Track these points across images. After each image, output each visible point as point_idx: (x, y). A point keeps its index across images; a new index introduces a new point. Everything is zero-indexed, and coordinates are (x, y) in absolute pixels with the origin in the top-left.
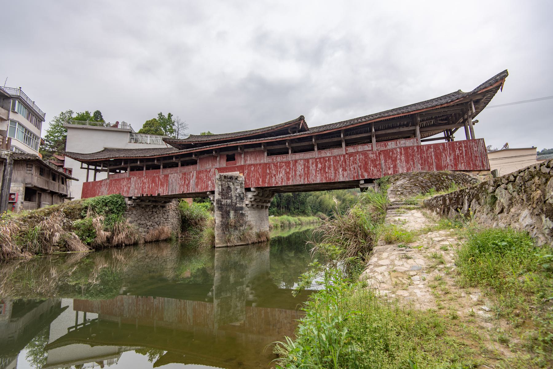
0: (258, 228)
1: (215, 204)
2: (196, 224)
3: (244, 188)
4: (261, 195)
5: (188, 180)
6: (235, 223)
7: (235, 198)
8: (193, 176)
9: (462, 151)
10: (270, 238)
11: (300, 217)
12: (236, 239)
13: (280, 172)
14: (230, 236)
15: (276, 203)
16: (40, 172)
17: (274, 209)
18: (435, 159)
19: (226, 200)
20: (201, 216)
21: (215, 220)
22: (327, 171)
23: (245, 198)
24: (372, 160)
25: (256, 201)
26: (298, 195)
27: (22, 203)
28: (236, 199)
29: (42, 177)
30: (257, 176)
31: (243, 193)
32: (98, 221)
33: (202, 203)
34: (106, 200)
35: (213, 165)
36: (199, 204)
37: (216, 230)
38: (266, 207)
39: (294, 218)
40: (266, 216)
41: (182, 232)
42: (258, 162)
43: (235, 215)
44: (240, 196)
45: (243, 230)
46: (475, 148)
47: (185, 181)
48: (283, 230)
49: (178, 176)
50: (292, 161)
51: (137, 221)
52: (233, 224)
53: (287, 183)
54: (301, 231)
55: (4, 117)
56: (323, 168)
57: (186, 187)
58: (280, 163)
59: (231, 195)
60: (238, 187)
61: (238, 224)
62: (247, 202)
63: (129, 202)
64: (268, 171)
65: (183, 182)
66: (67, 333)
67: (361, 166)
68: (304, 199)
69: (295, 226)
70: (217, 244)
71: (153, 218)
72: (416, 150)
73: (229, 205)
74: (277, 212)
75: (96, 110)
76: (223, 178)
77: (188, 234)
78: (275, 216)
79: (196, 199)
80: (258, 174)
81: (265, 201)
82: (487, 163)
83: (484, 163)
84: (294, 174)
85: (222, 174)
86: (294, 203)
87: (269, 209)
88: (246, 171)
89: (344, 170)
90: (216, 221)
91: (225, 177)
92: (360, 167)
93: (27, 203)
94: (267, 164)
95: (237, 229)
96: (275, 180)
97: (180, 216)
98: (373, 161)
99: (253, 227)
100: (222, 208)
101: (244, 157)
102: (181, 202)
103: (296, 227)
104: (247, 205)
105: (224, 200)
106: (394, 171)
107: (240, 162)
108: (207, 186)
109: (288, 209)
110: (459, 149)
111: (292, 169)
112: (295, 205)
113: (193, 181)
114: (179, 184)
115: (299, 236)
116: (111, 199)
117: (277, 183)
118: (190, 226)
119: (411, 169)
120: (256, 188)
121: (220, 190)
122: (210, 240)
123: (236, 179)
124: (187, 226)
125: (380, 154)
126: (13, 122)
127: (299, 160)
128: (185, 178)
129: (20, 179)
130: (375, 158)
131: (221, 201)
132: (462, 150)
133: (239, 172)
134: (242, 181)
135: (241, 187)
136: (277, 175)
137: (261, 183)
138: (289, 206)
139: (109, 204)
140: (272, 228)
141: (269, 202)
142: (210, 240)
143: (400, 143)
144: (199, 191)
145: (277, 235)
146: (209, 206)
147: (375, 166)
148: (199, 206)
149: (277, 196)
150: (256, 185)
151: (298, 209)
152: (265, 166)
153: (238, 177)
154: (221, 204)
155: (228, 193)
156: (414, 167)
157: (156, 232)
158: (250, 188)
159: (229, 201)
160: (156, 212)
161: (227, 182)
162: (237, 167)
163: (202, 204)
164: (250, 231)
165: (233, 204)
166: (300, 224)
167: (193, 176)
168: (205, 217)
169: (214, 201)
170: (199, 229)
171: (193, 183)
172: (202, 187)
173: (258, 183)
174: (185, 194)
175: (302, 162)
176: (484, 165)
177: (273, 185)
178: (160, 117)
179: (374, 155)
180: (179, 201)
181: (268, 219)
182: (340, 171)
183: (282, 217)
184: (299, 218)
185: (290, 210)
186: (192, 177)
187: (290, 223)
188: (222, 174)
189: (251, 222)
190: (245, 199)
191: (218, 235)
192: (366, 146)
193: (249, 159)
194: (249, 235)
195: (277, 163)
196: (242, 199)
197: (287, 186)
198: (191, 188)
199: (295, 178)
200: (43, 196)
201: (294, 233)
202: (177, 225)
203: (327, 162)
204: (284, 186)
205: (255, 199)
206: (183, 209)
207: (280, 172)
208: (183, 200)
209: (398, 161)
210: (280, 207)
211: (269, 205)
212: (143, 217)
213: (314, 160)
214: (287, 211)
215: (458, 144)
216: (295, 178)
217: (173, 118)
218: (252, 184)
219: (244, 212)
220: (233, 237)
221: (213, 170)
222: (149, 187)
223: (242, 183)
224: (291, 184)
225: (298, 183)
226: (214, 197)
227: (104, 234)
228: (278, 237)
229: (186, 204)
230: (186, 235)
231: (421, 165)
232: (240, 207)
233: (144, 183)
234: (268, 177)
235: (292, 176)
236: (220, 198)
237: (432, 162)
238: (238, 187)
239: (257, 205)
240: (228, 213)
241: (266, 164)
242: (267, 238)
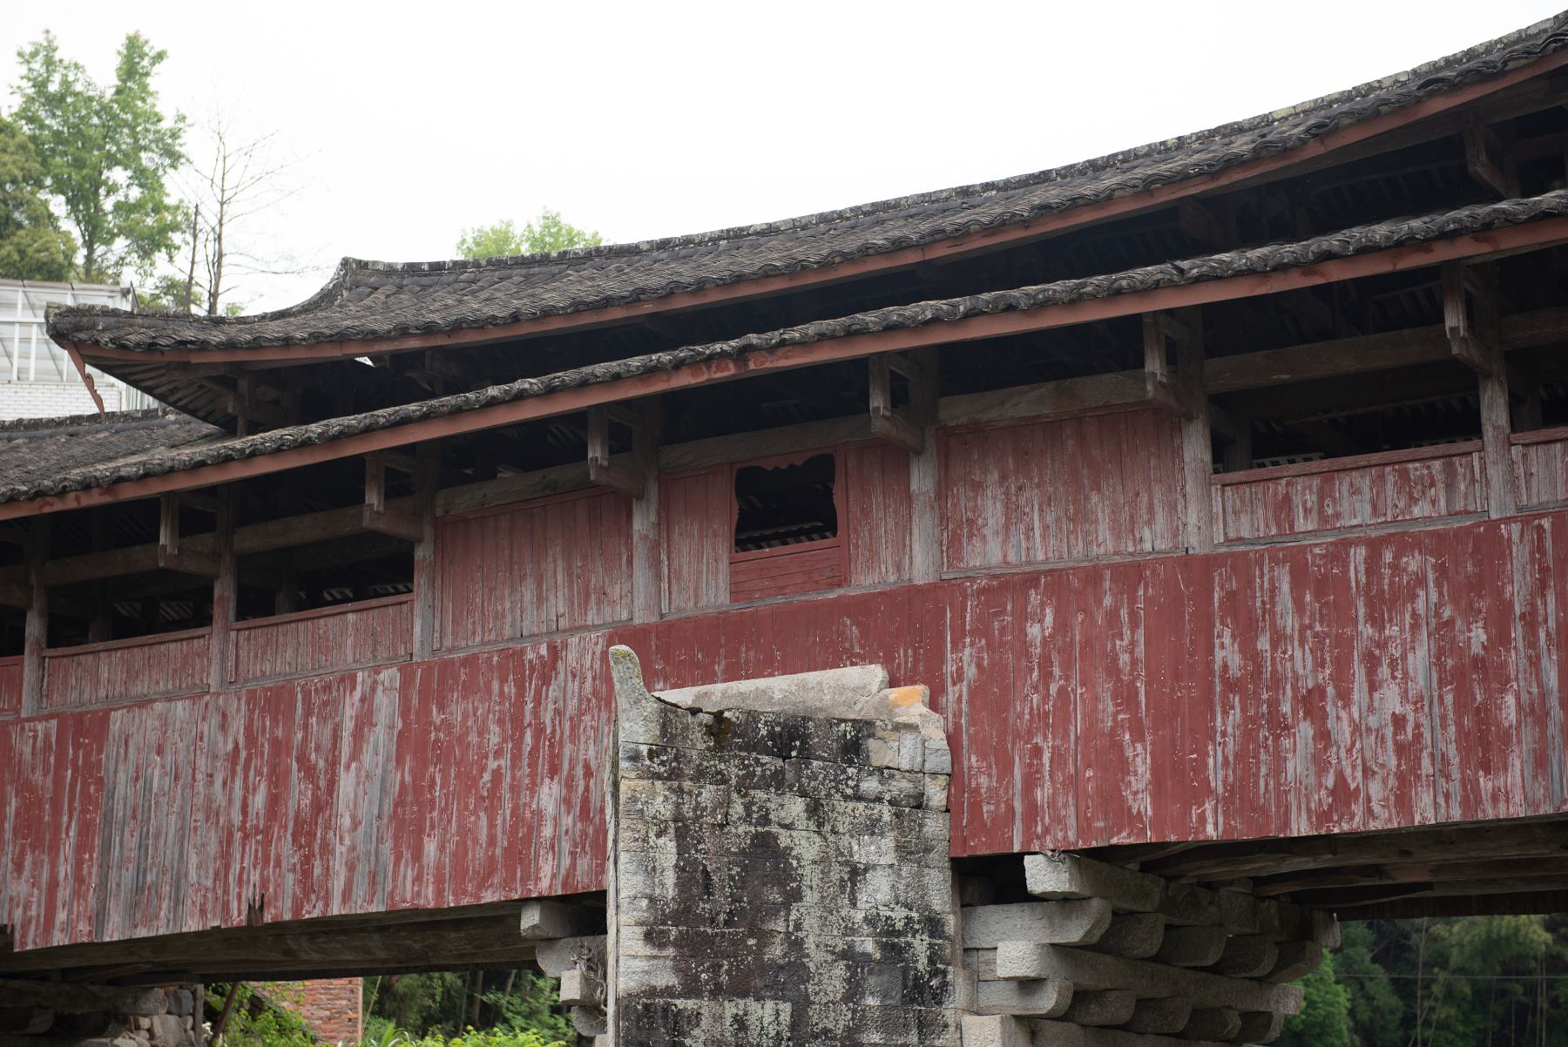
3: (939, 858)
7: (833, 981)
13: (1372, 662)
19: (730, 1009)
28: (854, 992)
44: (894, 950)
57: (286, 849)
60: (878, 851)
88: (964, 660)
101: (942, 491)
105: (706, 1006)
135: (903, 851)
137: (1144, 805)
155: (752, 919)
167: (364, 721)
223: (919, 802)
234: (1229, 722)
236: (666, 978)
238: (866, 850)
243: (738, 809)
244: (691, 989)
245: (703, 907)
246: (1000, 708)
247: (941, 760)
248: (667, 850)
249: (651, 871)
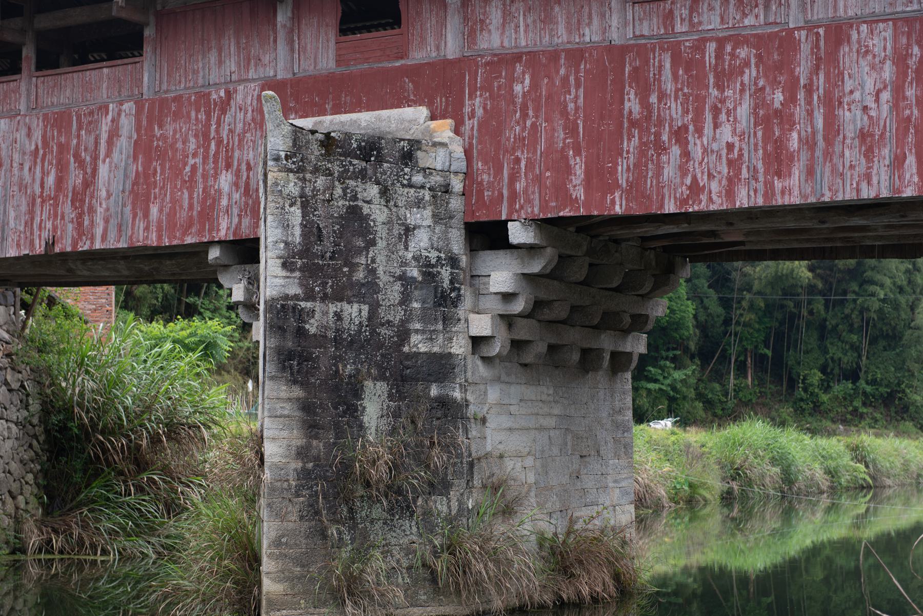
0: (553, 503)
1: (259, 331)
2: (141, 465)
4: (578, 272)
5: (81, 163)
6: (395, 467)
7: (394, 293)
8: (114, 134)
10: (645, 576)
11: (867, 439)
12: (403, 578)
13: (716, 111)
14: (362, 554)
15: (690, 330)
17: (678, 375)
18: (219, 158)
19: (332, 308)
20: (171, 413)
21: (258, 440)
23: (466, 291)
25: (547, 314)
26: (854, 274)
28: (405, 299)
30: (551, 141)
31: (453, 261)
33: (181, 323)
35: (247, 62)
36: (157, 328)
37: (264, 513)
38: (619, 361)
39: (822, 442)
40: (617, 425)
41: (48, 510)
42: (561, 36)
43: (396, 414)
44: (430, 275)
45: (449, 520)
47: (62, 168)
48: (736, 525)
49: (21, 135)
50: (811, 27)
52: (379, 473)
53: (769, 191)
54: (869, 532)
57: (67, 209)
58: (721, 42)
59: (372, 272)
60: (422, 217)
61: (417, 477)
62: (481, 325)
64: (632, 104)
65: (51, 180)
68: (896, 307)
69: (825, 501)
74: (700, 396)
76: (315, 151)
77: (85, 527)
78: (684, 422)
79: (141, 290)
80: (559, 123)
81: (605, 314)
84: (820, 123)
85: (307, 123)
86: (823, 331)
87: (640, 375)
88: (475, 105)
90: (269, 449)
91: (328, 142)
94: (624, 50)
95: (408, 510)
96: (683, 170)
97: (35, 406)
99: (517, 500)
100: (304, 358)
102: (40, 309)
103: (832, 508)
104: (477, 342)
105: (318, 306)
108: (208, 213)
109: (778, 379)
111: (809, 89)
112: (834, 351)
113: (114, 168)
114: (22, 187)
115: (857, 572)
117: (696, 189)
118: (97, 474)
120: (545, 224)
122: (224, 578)
124: (77, 477)
127: (795, 28)
128: (62, 148)
131: (302, 316)
133: (423, 112)
134: (445, 172)
135: (437, 218)
136: (699, 131)
137: (579, 193)
138: (790, 357)
140: (658, 508)
141: (638, 322)
142: (224, 578)
144: (153, 241)
145: (698, 559)
146: (225, 345)
148: (159, 341)
149: (703, 284)
150: (544, 207)
151: (853, 375)
153: (415, 144)
154: (301, 333)
155: (347, 256)
158: (502, 226)
159: (355, 312)
162: (415, 72)
163: (180, 328)
164: (500, 528)
165: (383, 331)
166: (863, 488)
167: (114, 134)
168: (198, 418)
169: (251, 306)
170: (156, 500)
171: (117, 187)
172: (172, 214)
173: (562, 193)
174: (63, 254)
177: (670, 207)
180: (25, 306)
181: (628, 448)
183: (733, 431)
184: (854, 439)
185: (792, 384)
186: (110, 143)
187: (788, 478)
188: (307, 123)
189: (509, 464)
190: (468, 301)
193: (495, 16)
194: (495, 556)
195: (699, 46)
197: (770, 213)
198: (99, 220)
199: (828, 155)
201: (814, 551)
202: (14, 466)
204: (750, 214)
205: (538, 305)
206: (52, 358)
207: (716, 111)
208: (51, 302)
210: (725, 358)
211: (638, 345)
214: (771, 387)
216: (828, 155)
218: (513, 195)
219: (457, 395)
220: (378, 562)
221: (244, 95)
224: (795, 199)
225: (847, 194)
226: (254, 282)
228: (702, 570)
229: (74, 328)
230: (76, 532)
232: (431, 357)
234: (631, 145)
235: (809, 143)
236: (294, 289)
238: (414, 217)
239: (552, 348)
241: (617, 53)
242: (617, 577)
243: (338, 191)
244: (310, 295)
245: (317, 249)
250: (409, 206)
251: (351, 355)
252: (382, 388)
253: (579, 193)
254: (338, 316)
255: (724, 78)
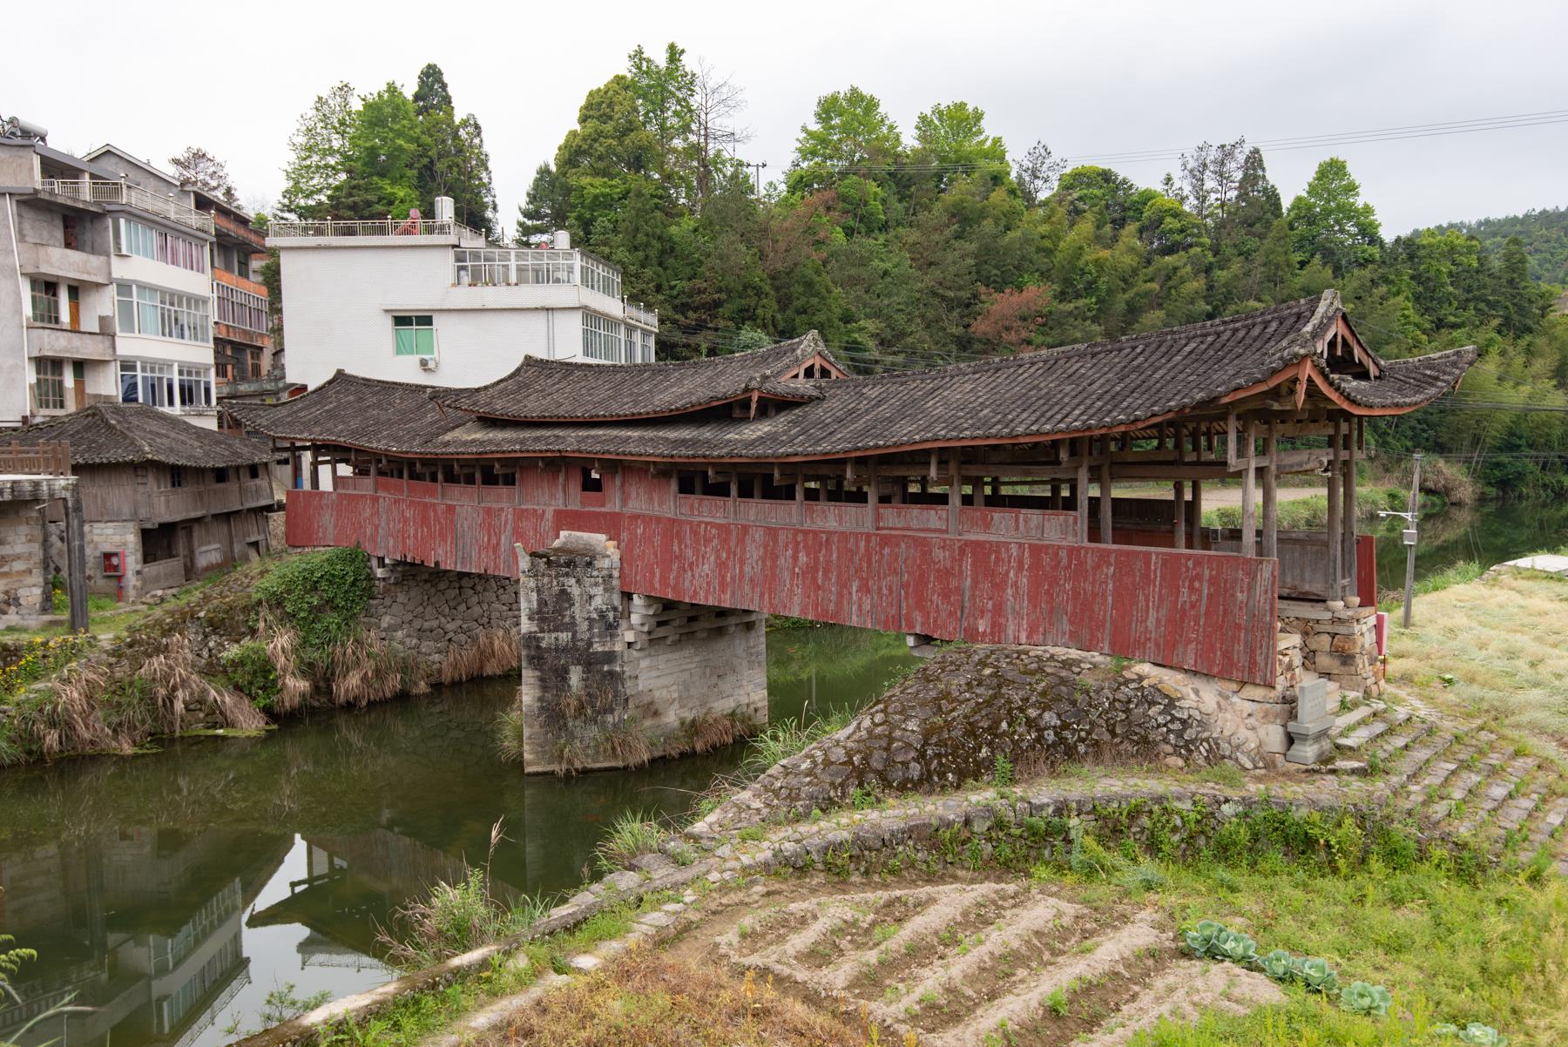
3: (617, 590)
7: (585, 625)
8: (506, 523)
9: (1200, 596)
13: (703, 558)
16: (173, 477)
19: (553, 635)
22: (820, 582)
24: (939, 571)
27: (138, 573)
28: (590, 628)
29: (179, 490)
32: (280, 643)
34: (312, 573)
44: (602, 615)
46: (1242, 592)
51: (410, 622)
55: (100, 280)
56: (811, 570)
57: (491, 553)
60: (599, 590)
62: (629, 636)
63: (380, 573)
66: (289, 894)
67: (908, 583)
70: (530, 764)
71: (462, 607)
72: (1065, 561)
73: (565, 650)
75: (425, 65)
82: (1267, 657)
83: (1258, 658)
88: (624, 535)
89: (865, 588)
92: (905, 586)
93: (154, 569)
96: (691, 582)
98: (944, 574)
100: (540, 658)
101: (623, 485)
104: (630, 644)
105: (546, 635)
106: (994, 624)
107: (613, 501)
110: (1191, 588)
116: (327, 567)
119: (1041, 629)
121: (535, 605)
123: (589, 564)
125: (962, 552)
126: (124, 287)
129: (126, 510)
130: (948, 565)
131: (538, 640)
132: (1200, 591)
135: (606, 590)
137: (657, 586)
139: (324, 585)
143: (1026, 522)
147: (945, 595)
152: (671, 528)
154: (538, 647)
155: (560, 611)
156: (1051, 624)
157: (468, 655)
159: (564, 637)
160: (472, 588)
161: (557, 576)
167: (506, 523)
175: (759, 535)
176: (1255, 663)
178: (639, 68)
179: (947, 553)
182: (854, 589)
191: (530, 738)
192: (932, 512)
196: (611, 628)
200: (197, 532)
203: (823, 552)
209: (1009, 591)
212: (429, 609)
213: (790, 536)
215: (1190, 564)
217: (688, 63)
222: (415, 536)
223: (611, 576)
227: (296, 686)
231: (1071, 623)
233: (405, 522)
234: (675, 567)
235: (733, 579)
236: (535, 629)
237: (1105, 616)
238: (593, 591)
240: (563, 674)
243: (555, 583)
244: (542, 631)
245: (545, 610)
246: (631, 551)
247: (617, 564)
248: (534, 596)
249: (529, 602)
250: (591, 586)
251: (563, 655)
252: (579, 668)
253: (657, 586)
254: (557, 639)
255: (707, 541)
